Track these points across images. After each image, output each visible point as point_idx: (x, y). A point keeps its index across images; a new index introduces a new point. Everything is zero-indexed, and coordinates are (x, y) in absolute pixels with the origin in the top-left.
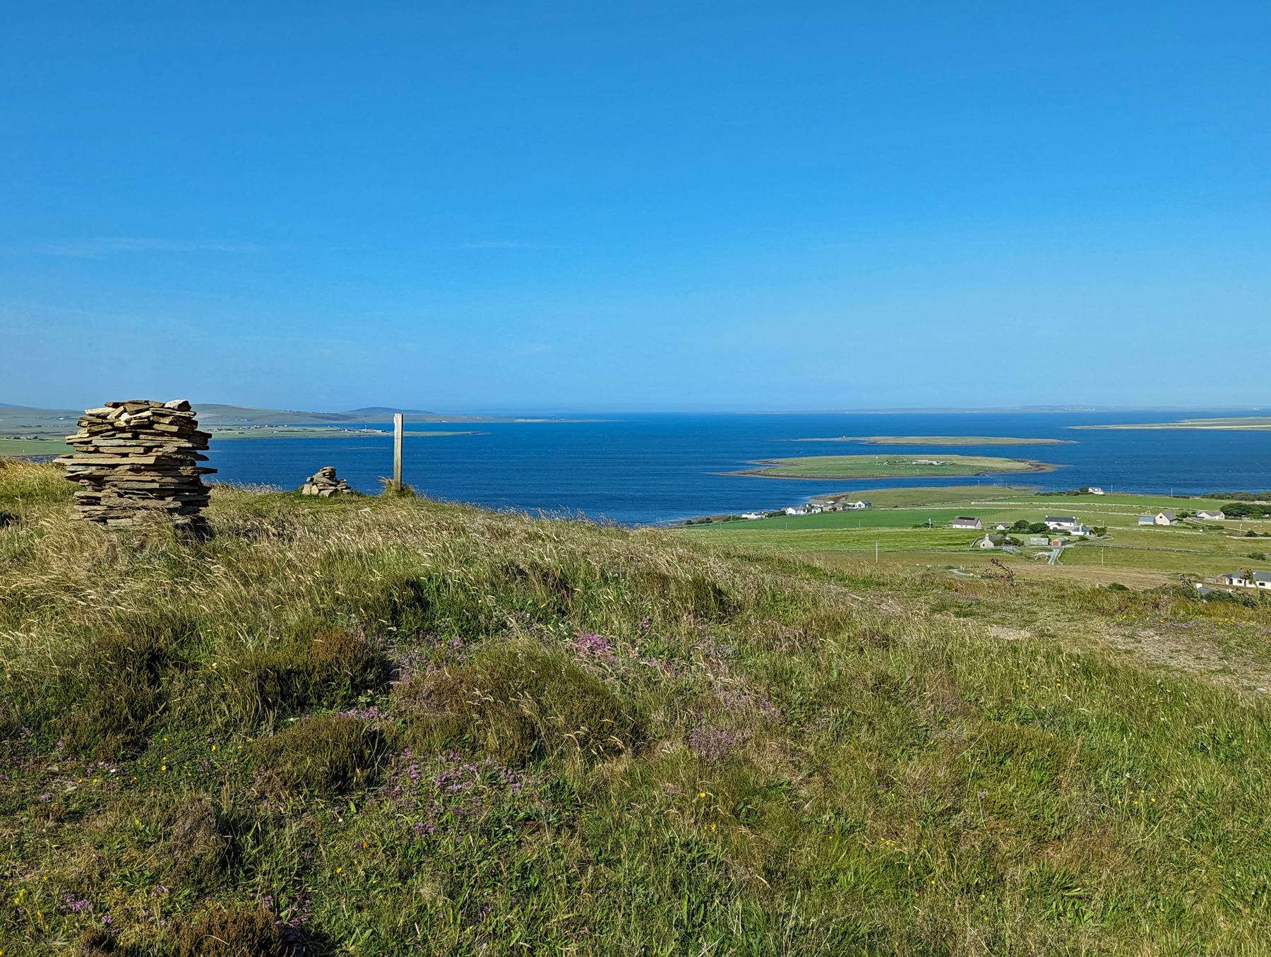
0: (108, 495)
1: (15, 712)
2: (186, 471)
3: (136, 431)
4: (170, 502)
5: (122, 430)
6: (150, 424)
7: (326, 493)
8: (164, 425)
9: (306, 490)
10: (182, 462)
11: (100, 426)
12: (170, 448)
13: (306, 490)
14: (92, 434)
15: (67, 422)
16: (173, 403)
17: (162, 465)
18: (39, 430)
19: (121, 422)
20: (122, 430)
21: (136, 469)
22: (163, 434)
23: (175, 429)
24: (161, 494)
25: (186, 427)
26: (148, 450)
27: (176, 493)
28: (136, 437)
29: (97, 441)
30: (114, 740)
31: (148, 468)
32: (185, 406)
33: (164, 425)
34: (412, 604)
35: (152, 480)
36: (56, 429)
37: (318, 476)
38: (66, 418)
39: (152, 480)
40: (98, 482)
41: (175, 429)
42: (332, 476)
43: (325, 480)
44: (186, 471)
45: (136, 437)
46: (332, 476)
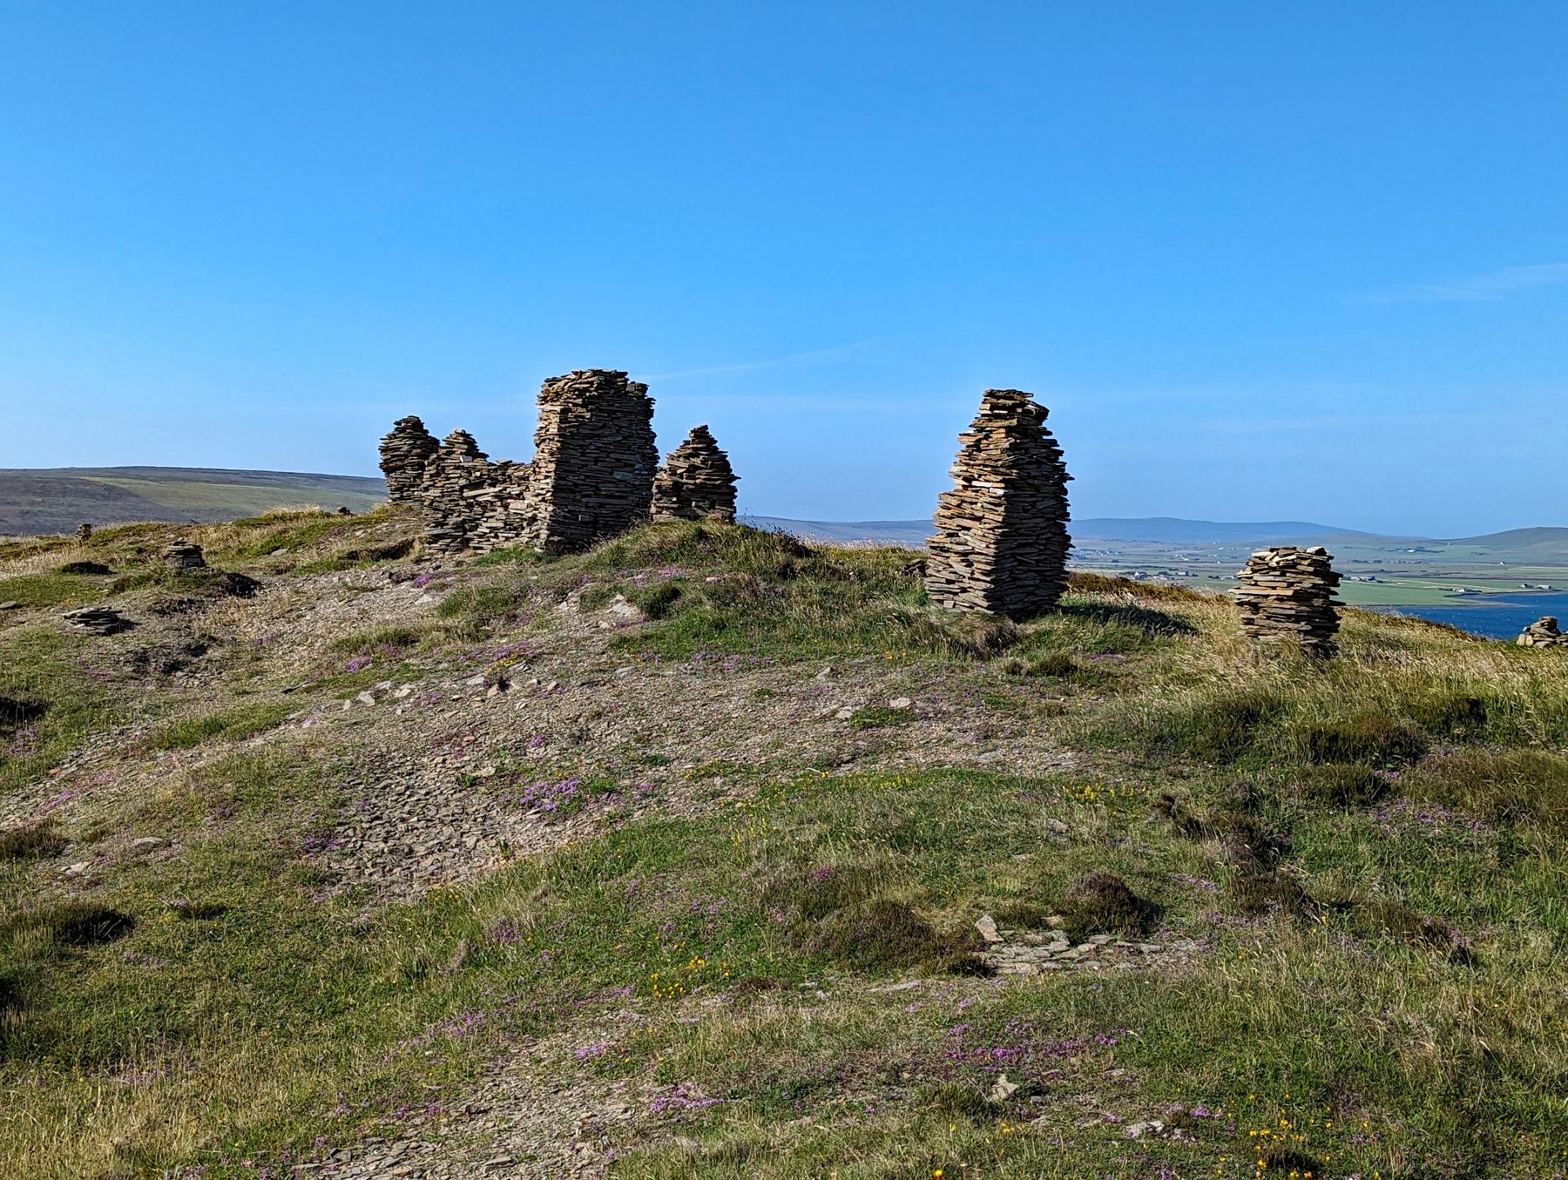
0: (1259, 618)
1: (1166, 730)
2: (1318, 602)
3: (1283, 570)
4: (1303, 626)
5: (1274, 569)
6: (1294, 565)
7: (1541, 645)
8: (1304, 566)
9: (1521, 641)
10: (1317, 596)
11: (1260, 566)
12: (1307, 584)
13: (1521, 641)
14: (1254, 571)
15: (1419, 556)
16: (1312, 550)
17: (1299, 597)
18: (1379, 567)
19: (1273, 564)
20: (1274, 569)
21: (1281, 599)
22: (1303, 573)
23: (1311, 569)
24: (1297, 618)
25: (1321, 566)
26: (1290, 585)
27: (1309, 619)
28: (1283, 574)
29: (1257, 577)
30: (1214, 752)
31: (1289, 598)
32: (1321, 552)
33: (1304, 566)
34: (1471, 713)
35: (1290, 608)
36: (1401, 567)
37: (1536, 627)
38: (1417, 550)
39: (1290, 608)
40: (1255, 607)
41: (1311, 569)
42: (1552, 626)
43: (1543, 630)
44: (1318, 602)
45: (1283, 574)
46: (1552, 626)
